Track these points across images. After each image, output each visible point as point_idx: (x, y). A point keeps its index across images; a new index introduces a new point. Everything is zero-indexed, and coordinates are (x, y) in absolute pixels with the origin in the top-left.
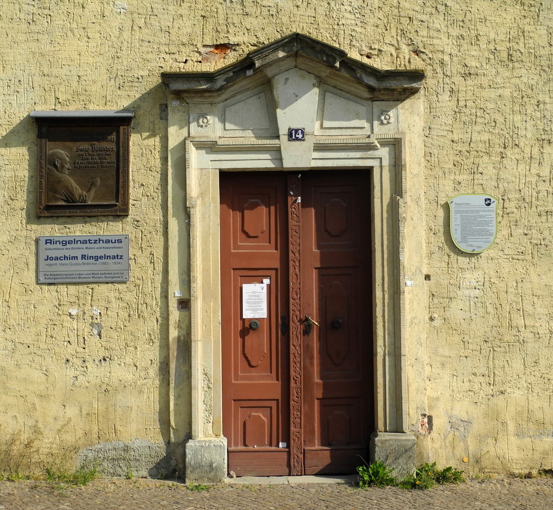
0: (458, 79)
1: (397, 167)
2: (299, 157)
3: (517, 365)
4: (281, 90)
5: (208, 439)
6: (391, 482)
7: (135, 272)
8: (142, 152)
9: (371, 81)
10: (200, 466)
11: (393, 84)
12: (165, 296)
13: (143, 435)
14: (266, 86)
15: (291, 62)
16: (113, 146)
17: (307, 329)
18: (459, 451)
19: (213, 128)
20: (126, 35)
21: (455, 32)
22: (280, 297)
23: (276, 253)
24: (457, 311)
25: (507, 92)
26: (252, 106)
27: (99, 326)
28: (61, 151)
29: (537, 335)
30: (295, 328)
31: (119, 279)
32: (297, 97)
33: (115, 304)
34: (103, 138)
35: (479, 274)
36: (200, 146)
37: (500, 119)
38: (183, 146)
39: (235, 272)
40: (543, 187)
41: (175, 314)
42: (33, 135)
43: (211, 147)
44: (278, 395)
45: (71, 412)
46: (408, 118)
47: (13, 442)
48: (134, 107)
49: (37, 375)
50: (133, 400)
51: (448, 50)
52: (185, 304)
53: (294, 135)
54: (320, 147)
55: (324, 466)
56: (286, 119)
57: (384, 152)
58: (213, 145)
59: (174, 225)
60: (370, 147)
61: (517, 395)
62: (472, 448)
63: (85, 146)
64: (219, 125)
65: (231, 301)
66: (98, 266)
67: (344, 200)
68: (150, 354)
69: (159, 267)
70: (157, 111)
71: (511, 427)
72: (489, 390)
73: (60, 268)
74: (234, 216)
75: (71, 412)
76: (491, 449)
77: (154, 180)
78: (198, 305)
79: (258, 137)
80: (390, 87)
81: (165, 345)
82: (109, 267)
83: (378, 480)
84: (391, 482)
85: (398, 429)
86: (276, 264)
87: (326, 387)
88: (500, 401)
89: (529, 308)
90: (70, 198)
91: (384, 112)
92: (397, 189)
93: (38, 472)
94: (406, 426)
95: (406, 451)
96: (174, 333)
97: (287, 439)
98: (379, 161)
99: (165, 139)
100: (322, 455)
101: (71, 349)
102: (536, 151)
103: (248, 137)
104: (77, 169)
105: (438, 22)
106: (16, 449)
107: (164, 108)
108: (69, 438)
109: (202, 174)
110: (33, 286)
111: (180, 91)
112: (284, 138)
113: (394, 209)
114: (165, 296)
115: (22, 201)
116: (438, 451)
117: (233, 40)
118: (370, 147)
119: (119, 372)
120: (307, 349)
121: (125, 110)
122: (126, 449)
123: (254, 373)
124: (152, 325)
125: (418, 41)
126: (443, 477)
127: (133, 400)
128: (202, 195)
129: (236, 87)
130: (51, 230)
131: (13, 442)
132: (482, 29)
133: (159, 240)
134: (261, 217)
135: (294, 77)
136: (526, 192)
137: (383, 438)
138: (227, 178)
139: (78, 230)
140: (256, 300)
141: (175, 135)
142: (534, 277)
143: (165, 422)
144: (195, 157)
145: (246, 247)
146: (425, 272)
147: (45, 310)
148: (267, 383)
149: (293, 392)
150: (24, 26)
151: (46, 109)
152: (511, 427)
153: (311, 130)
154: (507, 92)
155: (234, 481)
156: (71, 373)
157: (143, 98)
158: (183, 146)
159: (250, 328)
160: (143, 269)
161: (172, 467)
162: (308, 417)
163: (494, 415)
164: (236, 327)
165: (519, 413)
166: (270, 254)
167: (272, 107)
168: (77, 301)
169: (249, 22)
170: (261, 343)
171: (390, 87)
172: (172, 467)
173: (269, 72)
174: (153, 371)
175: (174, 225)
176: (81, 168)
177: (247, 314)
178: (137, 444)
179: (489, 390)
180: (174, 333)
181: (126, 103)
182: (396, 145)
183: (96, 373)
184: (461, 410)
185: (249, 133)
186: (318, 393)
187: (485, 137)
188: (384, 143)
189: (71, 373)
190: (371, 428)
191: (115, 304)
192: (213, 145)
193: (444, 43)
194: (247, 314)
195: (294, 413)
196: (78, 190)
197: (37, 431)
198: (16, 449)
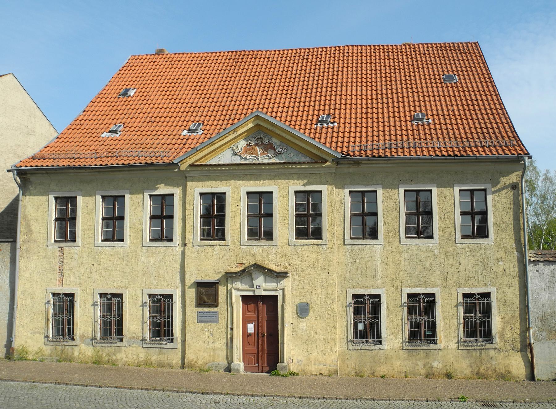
0: (300, 272)
1: (284, 295)
2: (259, 292)
3: (315, 346)
4: (254, 276)
5: (239, 363)
6: (279, 375)
7: (220, 321)
8: (222, 290)
9: (276, 274)
10: (234, 369)
11: (281, 275)
12: (227, 327)
13: (223, 362)
14: (250, 275)
15: (255, 269)
16: (214, 289)
17: (263, 336)
18: (299, 368)
19: (238, 285)
20: (218, 260)
21: (300, 259)
22: (257, 327)
23: (256, 316)
24: (299, 333)
25: (313, 276)
26: (248, 279)
27: (212, 334)
28: (203, 290)
29: (320, 339)
30: (260, 336)
31: (216, 322)
32: (258, 278)
33: (216, 328)
34: (212, 287)
35: (305, 323)
36: (235, 289)
37: (311, 282)
38: (231, 289)
39: (246, 321)
40: (322, 301)
41: (229, 331)
42: (196, 286)
43: (238, 290)
44: (256, 352)
45: (206, 354)
46: (287, 283)
47: (192, 361)
48: (219, 280)
49: (198, 345)
50: (220, 353)
51: (298, 264)
52: (232, 329)
53: (258, 287)
54: (264, 290)
55: (7, 315)
56: (256, 283)
57: (281, 291)
58: (237, 290)
59: (229, 309)
60: (277, 290)
61: (314, 354)
62: (302, 367)
63: (208, 289)
64: (240, 284)
65: (245, 328)
66: (211, 319)
67: (271, 302)
68: (224, 341)
69: (226, 320)
70: (225, 280)
71: (313, 362)
72: (308, 353)
73: (203, 319)
74: (246, 306)
75: (206, 354)
76: (307, 368)
77: (225, 298)
78: (235, 330)
79: (250, 287)
80: (282, 276)
81: (227, 339)
82: (213, 319)
83: (276, 375)
84: (279, 375)
85: (283, 362)
86: (256, 319)
87: (268, 351)
88: (310, 356)
89: (318, 332)
90: (204, 302)
91: (281, 281)
92: (284, 301)
93: (197, 369)
94: (285, 361)
95: (284, 367)
96: (229, 336)
97: (258, 363)
98: (279, 293)
99: (227, 287)
100: (267, 368)
101: (205, 339)
102: (320, 291)
103: (247, 287)
104: (206, 295)
105: (295, 257)
106: (193, 363)
107: (227, 279)
108: (205, 361)
109: (236, 297)
110: (197, 323)
111: (230, 276)
112: (255, 288)
113: (283, 306)
114: (227, 327)
115: (194, 302)
116: (293, 368)
117: (244, 262)
118: (277, 290)
119: (217, 345)
120: (263, 341)
121: (217, 280)
122: (218, 364)
123: (250, 346)
124: (224, 334)
125: (290, 262)
126: (292, 374)
127: (220, 353)
128: (236, 302)
129: (244, 275)
130: (201, 309)
131: (192, 361)
132: (307, 259)
133: (226, 312)
134: (252, 306)
135: (257, 273)
136: (318, 302)
137: (279, 364)
138: (243, 297)
139: (207, 310)
140: (251, 328)
141: (229, 286)
142: (319, 324)
143: (227, 358)
144: (234, 292)
145: (249, 314)
146: (291, 322)
147: (199, 329)
148: (253, 349)
149: (260, 352)
150: (194, 258)
151: (200, 279)
152: (313, 362)
153: (262, 286)
154: (313, 276)
155: (245, 373)
156: (206, 345)
157: (222, 277)
158: (231, 289)
159: (249, 335)
160: (222, 319)
161: (229, 369)
162: (263, 358)
163: (309, 359)
164: (246, 335)
165: (315, 359)
166: (254, 316)
167: (252, 280)
168: (207, 327)
169: (247, 257)
170: (252, 339)
171: (282, 276)
172: (229, 369)
173: (251, 272)
174: (225, 345)
175: (229, 309)
176: (207, 295)
177: (249, 332)
178: (221, 363)
179: (308, 353)
180: (229, 336)
181: (218, 278)
182: (283, 290)
183: (211, 345)
184: (300, 358)
185: (247, 286)
186: (266, 352)
187: (307, 287)
188: (280, 289)
189: (206, 345)
190: (277, 362)
191: (216, 328)
192: (237, 290)
193: (297, 263)
194: (249, 332)
195: (260, 357)
196: (207, 300)
197: (198, 359)
198: (193, 363)
